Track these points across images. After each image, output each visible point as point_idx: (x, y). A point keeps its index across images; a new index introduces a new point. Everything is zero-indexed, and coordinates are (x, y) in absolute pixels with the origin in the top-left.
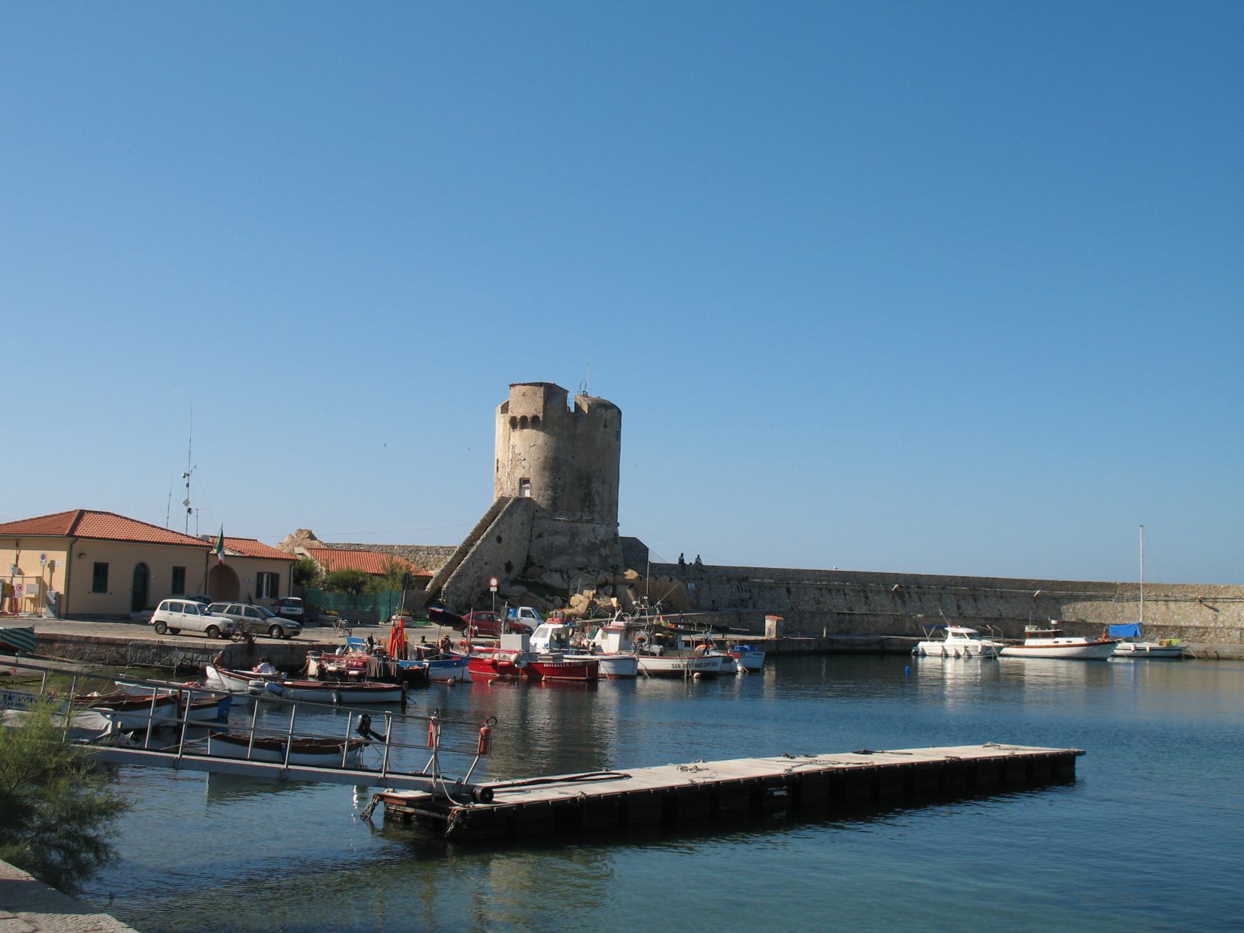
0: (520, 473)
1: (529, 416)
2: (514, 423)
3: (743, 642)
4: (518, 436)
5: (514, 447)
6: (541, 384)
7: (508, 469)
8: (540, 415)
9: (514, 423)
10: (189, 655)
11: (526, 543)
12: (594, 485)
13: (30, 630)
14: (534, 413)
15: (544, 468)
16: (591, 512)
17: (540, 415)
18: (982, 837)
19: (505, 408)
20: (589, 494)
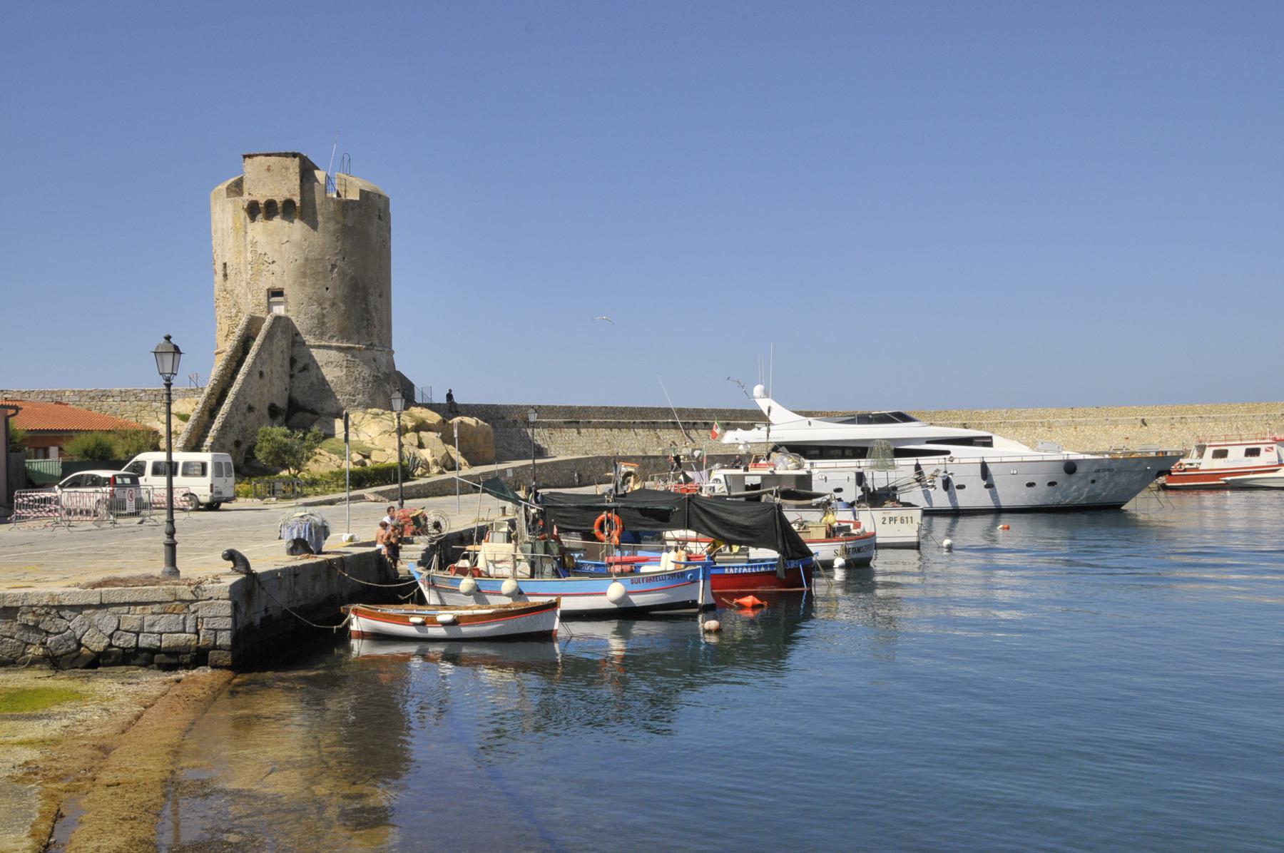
0: (268, 282)
1: (279, 200)
2: (253, 210)
3: (580, 485)
4: (260, 229)
5: (254, 244)
6: (295, 155)
7: (247, 276)
8: (297, 199)
9: (253, 210)
10: (132, 619)
11: (287, 379)
12: (371, 298)
13: (251, 624)
14: (287, 195)
15: (304, 275)
16: (370, 335)
17: (297, 199)
18: (965, 669)
19: (237, 188)
20: (367, 310)
